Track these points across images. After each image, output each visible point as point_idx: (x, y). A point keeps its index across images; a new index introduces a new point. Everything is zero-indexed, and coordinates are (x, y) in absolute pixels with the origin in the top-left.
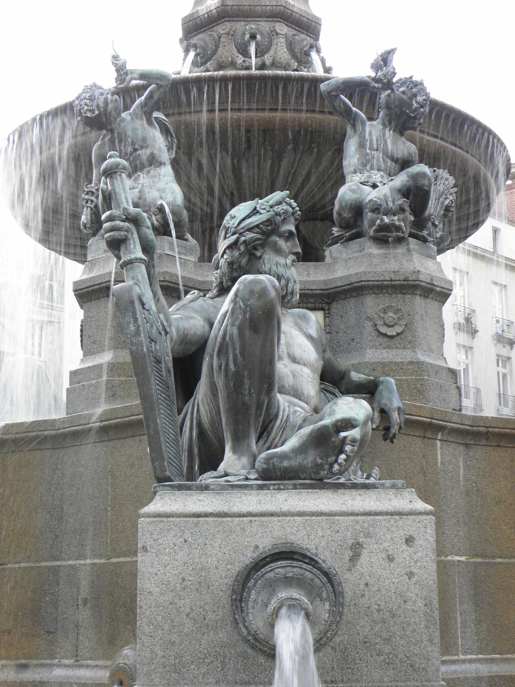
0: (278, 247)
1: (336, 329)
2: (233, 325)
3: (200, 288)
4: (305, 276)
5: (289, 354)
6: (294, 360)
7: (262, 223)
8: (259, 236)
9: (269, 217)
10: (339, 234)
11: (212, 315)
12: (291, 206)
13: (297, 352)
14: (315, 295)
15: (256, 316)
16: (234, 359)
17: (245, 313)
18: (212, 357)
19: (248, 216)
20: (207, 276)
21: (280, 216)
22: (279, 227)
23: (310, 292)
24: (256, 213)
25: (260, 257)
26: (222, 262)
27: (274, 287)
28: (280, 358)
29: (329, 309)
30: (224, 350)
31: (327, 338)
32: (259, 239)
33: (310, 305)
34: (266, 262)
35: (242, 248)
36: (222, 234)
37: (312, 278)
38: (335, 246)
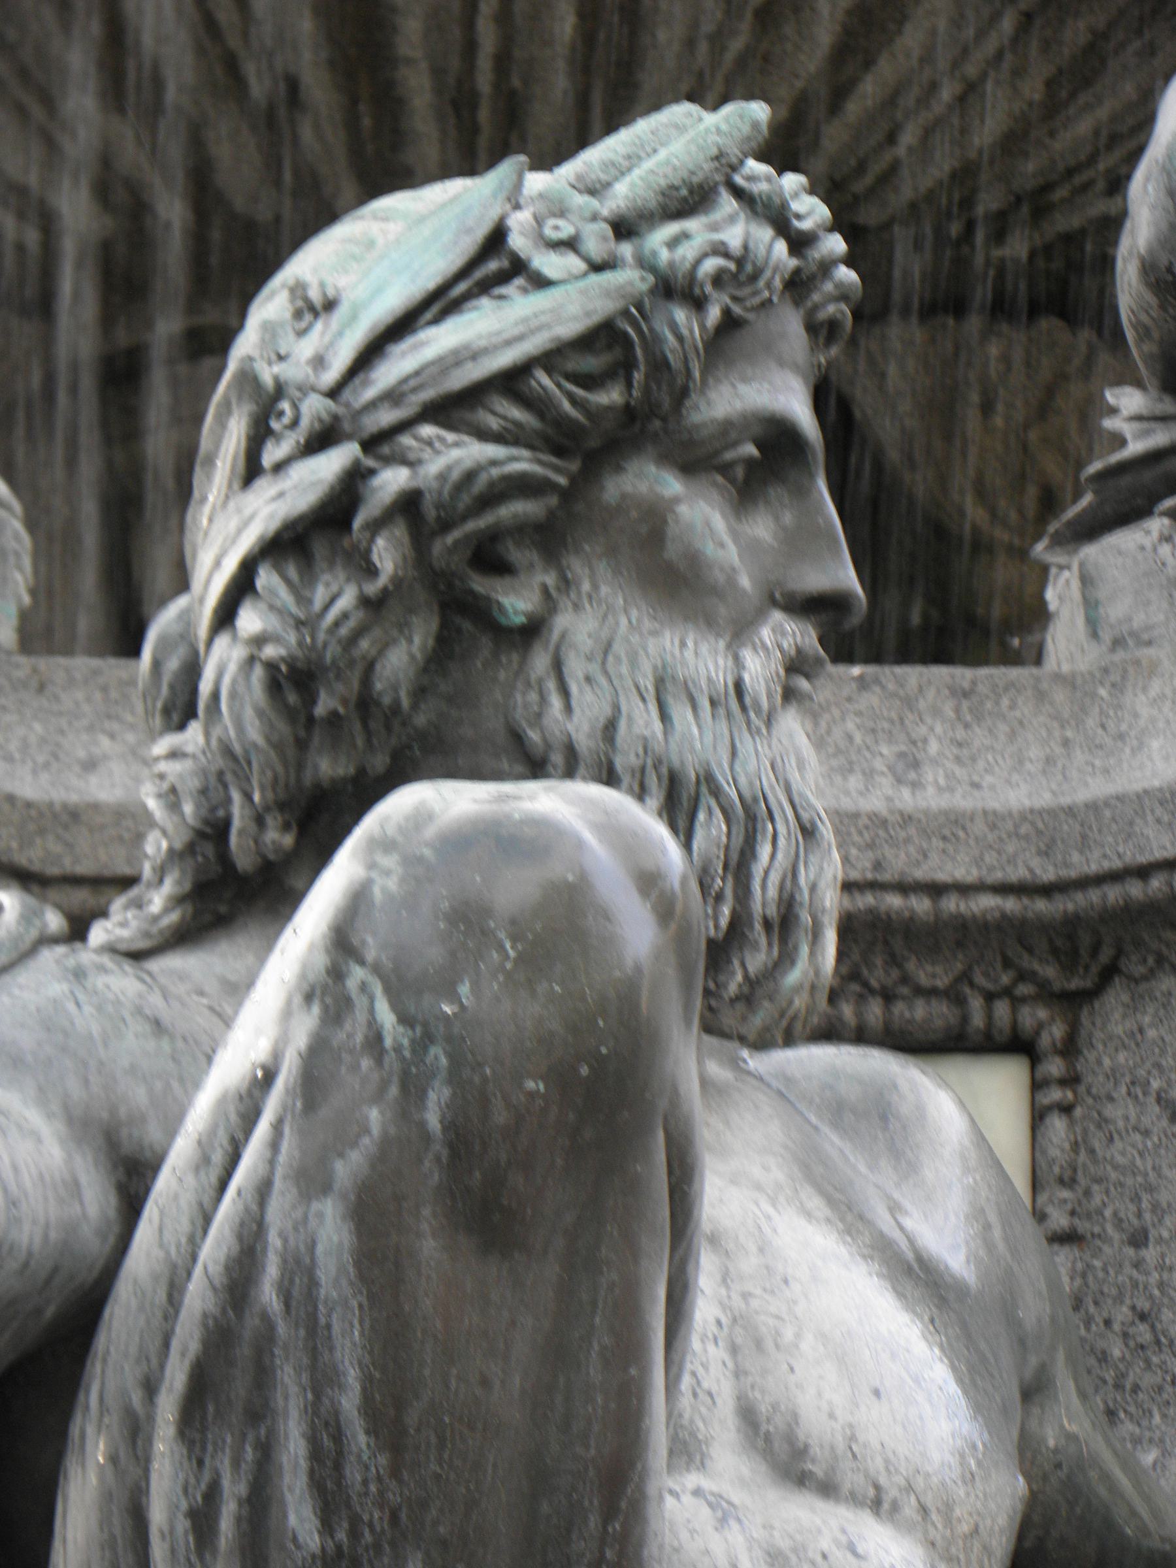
0: (672, 551)
1: (1128, 1211)
2: (312, 1181)
3: (31, 857)
4: (874, 778)
5: (748, 1416)
6: (794, 1463)
7: (549, 359)
8: (522, 462)
9: (603, 308)
10: (1160, 438)
11: (139, 1096)
12: (780, 220)
13: (818, 1399)
14: (964, 932)
15: (500, 1116)
16: (316, 1454)
17: (412, 1088)
18: (136, 1432)
19: (439, 303)
20: (90, 765)
21: (698, 304)
22: (682, 394)
23: (921, 905)
24: (503, 278)
25: (532, 631)
26: (223, 660)
27: (648, 881)
28: (688, 1451)
29: (1070, 1048)
30: (240, 1388)
31: (1053, 1284)
32: (521, 486)
33: (919, 1013)
34: (575, 668)
35: (387, 555)
36: (228, 439)
37: (931, 796)
38: (1127, 539)
